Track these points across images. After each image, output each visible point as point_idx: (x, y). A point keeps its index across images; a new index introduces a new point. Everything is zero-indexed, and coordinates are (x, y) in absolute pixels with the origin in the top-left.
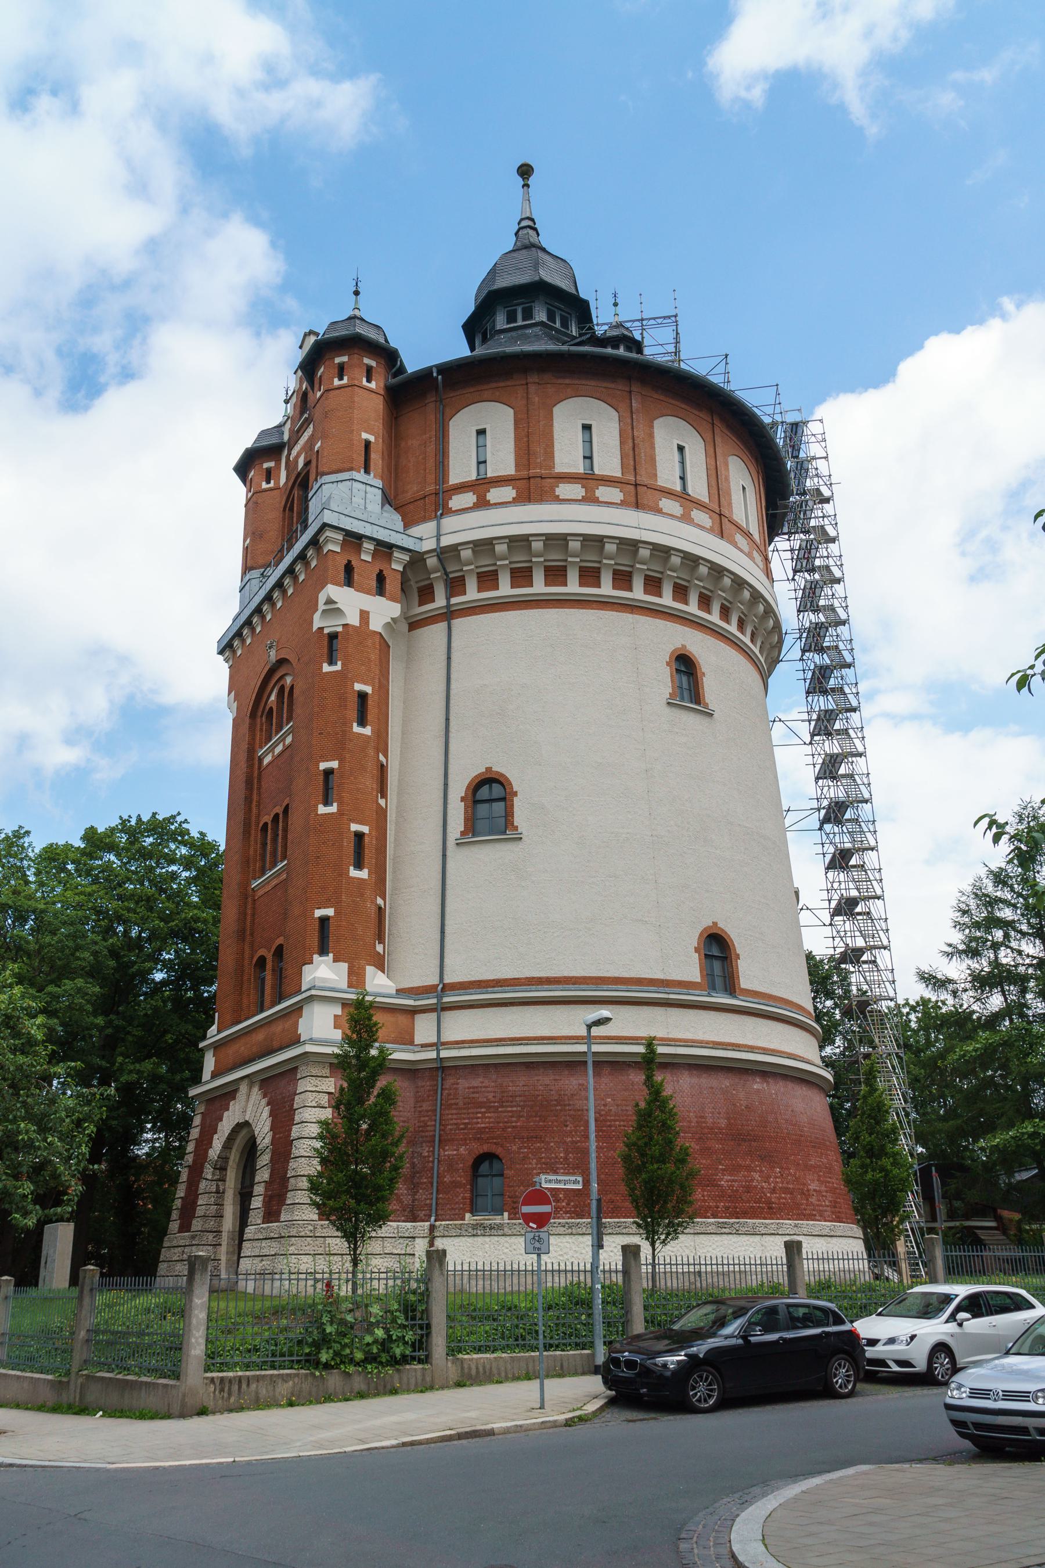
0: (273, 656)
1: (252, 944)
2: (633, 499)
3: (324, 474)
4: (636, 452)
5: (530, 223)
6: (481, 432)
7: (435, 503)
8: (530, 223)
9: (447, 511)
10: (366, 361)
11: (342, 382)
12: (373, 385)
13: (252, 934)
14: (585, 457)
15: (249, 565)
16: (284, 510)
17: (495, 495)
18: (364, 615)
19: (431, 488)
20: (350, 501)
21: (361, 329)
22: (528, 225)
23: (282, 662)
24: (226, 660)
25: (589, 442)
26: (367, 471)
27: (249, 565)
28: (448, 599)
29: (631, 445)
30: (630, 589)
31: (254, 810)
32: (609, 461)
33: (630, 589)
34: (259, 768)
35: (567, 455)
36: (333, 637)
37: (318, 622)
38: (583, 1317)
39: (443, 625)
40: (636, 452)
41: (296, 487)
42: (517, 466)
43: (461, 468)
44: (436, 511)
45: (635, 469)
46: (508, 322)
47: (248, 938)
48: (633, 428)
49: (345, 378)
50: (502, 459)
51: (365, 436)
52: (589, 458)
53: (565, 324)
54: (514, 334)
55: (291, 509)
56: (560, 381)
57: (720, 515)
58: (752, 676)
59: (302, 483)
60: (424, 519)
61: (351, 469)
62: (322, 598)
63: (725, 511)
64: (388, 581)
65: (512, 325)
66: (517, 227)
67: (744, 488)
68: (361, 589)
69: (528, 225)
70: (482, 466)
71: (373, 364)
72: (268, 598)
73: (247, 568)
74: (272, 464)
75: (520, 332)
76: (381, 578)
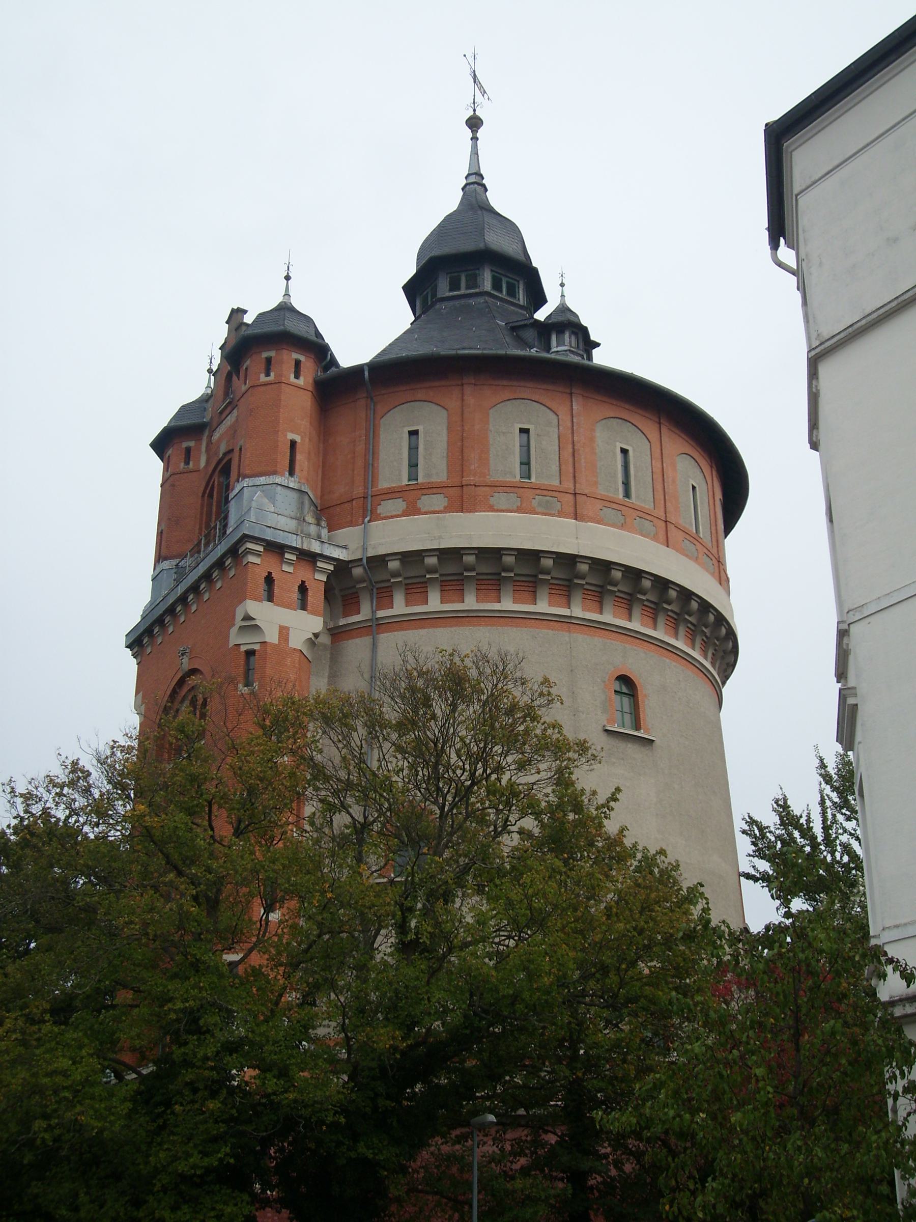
0: (186, 664)
2: (572, 509)
4: (572, 455)
5: (477, 179)
6: (414, 433)
7: (362, 507)
8: (477, 179)
9: (376, 517)
10: (295, 356)
11: (268, 379)
12: (301, 382)
14: (521, 464)
15: (163, 554)
16: (203, 496)
17: (426, 502)
18: (284, 632)
19: (359, 491)
20: (270, 506)
21: (292, 326)
22: (475, 184)
23: (193, 672)
24: (135, 656)
26: (292, 473)
27: (163, 554)
28: (374, 612)
29: (571, 450)
35: (504, 462)
36: (250, 653)
37: (235, 638)
39: (367, 640)
40: (572, 455)
41: (217, 473)
42: (449, 471)
43: (392, 470)
44: (364, 517)
45: (575, 477)
46: (451, 290)
48: (573, 433)
49: (272, 374)
50: (435, 465)
51: (291, 436)
53: (512, 292)
54: (456, 303)
55: (211, 495)
56: (496, 383)
57: (666, 521)
59: (224, 472)
60: (352, 524)
61: (275, 473)
62: (239, 615)
63: (671, 518)
64: (310, 593)
65: (455, 293)
66: (464, 182)
67: (694, 488)
69: (475, 184)
71: (302, 358)
72: (183, 599)
73: (160, 557)
74: (192, 444)
75: (462, 302)
76: (303, 589)
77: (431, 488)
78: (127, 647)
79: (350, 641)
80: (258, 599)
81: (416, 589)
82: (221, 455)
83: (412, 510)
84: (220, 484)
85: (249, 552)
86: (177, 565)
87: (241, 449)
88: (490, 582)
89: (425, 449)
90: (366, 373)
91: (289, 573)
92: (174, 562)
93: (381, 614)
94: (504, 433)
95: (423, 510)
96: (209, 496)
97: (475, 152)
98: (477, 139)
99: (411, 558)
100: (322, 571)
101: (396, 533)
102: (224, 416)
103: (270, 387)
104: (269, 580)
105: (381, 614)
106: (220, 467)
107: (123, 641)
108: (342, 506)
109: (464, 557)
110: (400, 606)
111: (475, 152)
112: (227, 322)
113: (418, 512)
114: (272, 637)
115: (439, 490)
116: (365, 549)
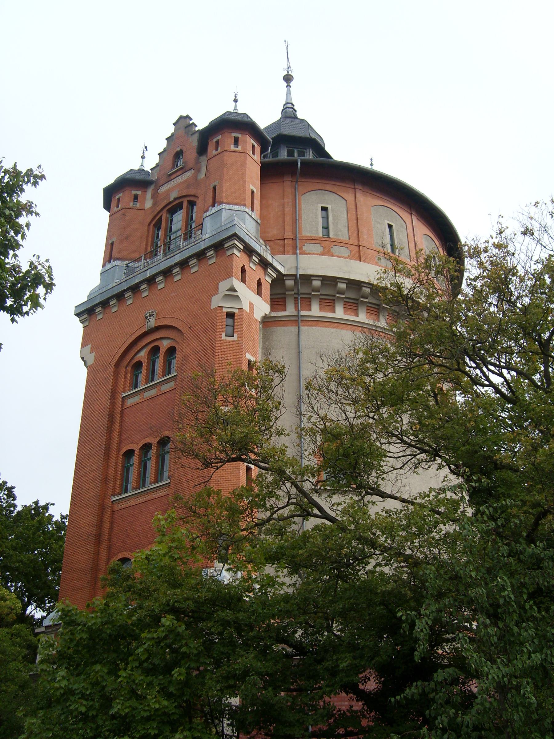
1: (109, 548)
7: (291, 243)
11: (236, 149)
13: (109, 539)
16: (149, 225)
17: (335, 249)
24: (82, 322)
32: (340, 228)
34: (122, 406)
37: (216, 301)
38: (494, 421)
39: (293, 329)
40: (356, 224)
47: (105, 542)
61: (244, 205)
62: (223, 286)
68: (249, 288)
70: (325, 226)
73: (109, 257)
74: (139, 193)
76: (259, 284)
77: (339, 243)
78: (77, 315)
79: (278, 328)
81: (328, 302)
82: (172, 199)
83: (327, 253)
85: (234, 246)
90: (299, 164)
91: (254, 271)
92: (125, 263)
93: (303, 313)
95: (335, 254)
97: (289, 93)
98: (290, 87)
99: (329, 281)
100: (270, 276)
101: (315, 264)
102: (173, 177)
103: (238, 153)
104: (243, 270)
105: (303, 313)
106: (169, 207)
108: (276, 241)
110: (315, 310)
111: (289, 93)
112: (174, 124)
113: (331, 254)
115: (344, 245)
116: (297, 268)
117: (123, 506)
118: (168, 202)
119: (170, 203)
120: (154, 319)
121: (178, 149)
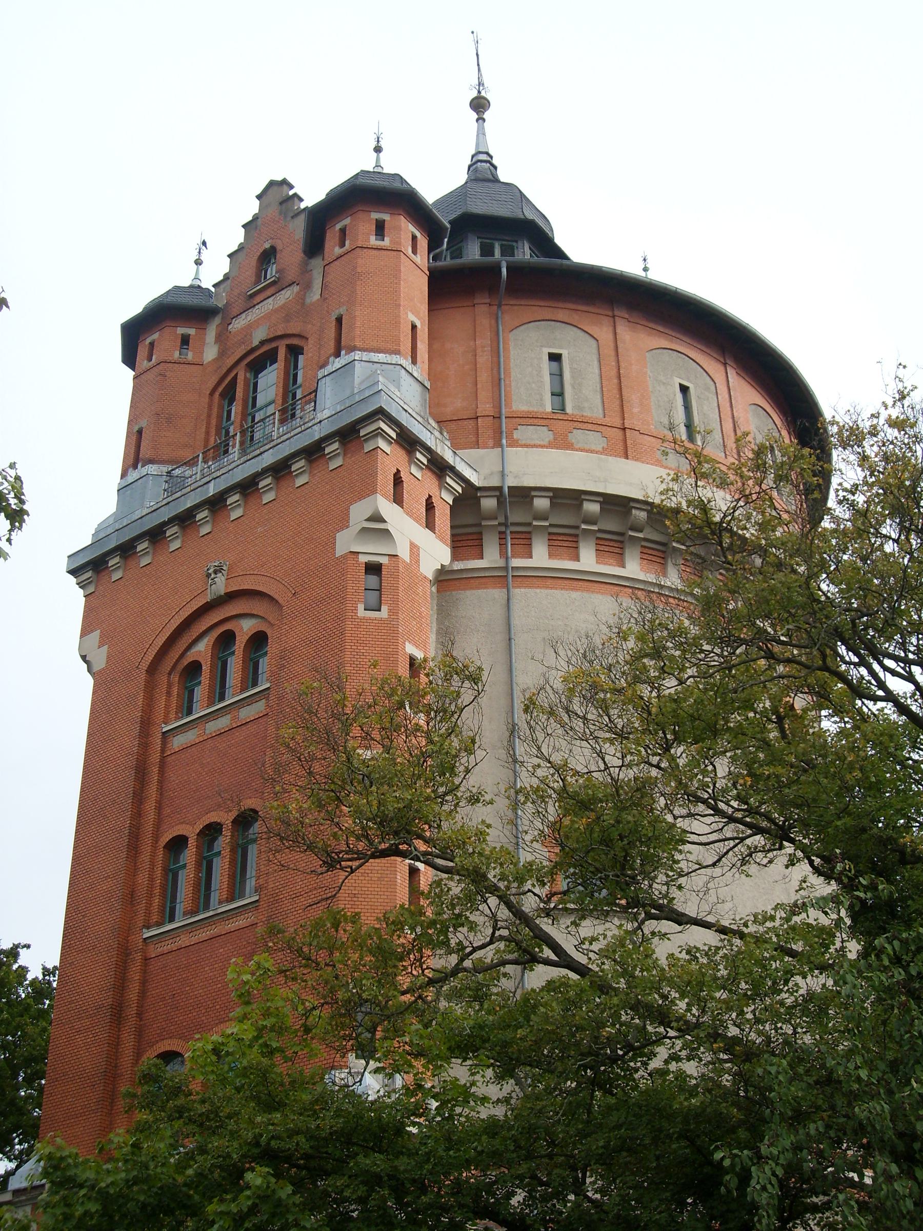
1: (140, 1033)
3: (352, 349)
7: (490, 425)
11: (380, 243)
12: (418, 259)
13: (140, 1015)
16: (212, 394)
17: (577, 436)
25: (558, 376)
30: (577, 558)
31: (150, 806)
33: (577, 558)
35: (528, 386)
37: (345, 542)
39: (498, 594)
47: (131, 1021)
52: (558, 394)
58: (97, 644)
61: (397, 352)
74: (192, 331)
76: (430, 506)
77: (583, 423)
79: (468, 593)
80: (385, 496)
81: (566, 540)
84: (247, 382)
85: (379, 433)
86: (169, 472)
87: (339, 320)
88: (650, 552)
89: (573, 377)
92: (165, 469)
93: (516, 562)
94: (664, 384)
96: (222, 395)
97: (481, 133)
98: (484, 120)
100: (450, 490)
104: (398, 480)
105: (516, 562)
107: (63, 564)
109: (634, 511)
110: (540, 556)
112: (259, 197)
113: (569, 446)
114: (404, 553)
116: (503, 474)
117: (166, 949)
118: (249, 348)
119: (253, 350)
120: (223, 579)
121: (267, 246)
